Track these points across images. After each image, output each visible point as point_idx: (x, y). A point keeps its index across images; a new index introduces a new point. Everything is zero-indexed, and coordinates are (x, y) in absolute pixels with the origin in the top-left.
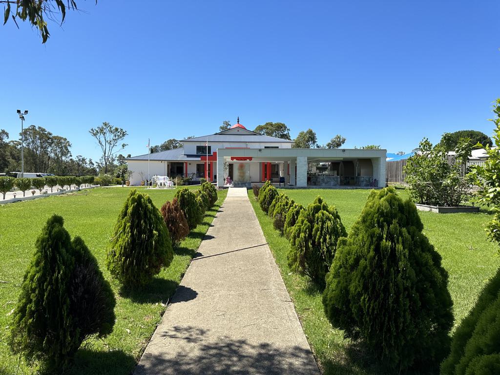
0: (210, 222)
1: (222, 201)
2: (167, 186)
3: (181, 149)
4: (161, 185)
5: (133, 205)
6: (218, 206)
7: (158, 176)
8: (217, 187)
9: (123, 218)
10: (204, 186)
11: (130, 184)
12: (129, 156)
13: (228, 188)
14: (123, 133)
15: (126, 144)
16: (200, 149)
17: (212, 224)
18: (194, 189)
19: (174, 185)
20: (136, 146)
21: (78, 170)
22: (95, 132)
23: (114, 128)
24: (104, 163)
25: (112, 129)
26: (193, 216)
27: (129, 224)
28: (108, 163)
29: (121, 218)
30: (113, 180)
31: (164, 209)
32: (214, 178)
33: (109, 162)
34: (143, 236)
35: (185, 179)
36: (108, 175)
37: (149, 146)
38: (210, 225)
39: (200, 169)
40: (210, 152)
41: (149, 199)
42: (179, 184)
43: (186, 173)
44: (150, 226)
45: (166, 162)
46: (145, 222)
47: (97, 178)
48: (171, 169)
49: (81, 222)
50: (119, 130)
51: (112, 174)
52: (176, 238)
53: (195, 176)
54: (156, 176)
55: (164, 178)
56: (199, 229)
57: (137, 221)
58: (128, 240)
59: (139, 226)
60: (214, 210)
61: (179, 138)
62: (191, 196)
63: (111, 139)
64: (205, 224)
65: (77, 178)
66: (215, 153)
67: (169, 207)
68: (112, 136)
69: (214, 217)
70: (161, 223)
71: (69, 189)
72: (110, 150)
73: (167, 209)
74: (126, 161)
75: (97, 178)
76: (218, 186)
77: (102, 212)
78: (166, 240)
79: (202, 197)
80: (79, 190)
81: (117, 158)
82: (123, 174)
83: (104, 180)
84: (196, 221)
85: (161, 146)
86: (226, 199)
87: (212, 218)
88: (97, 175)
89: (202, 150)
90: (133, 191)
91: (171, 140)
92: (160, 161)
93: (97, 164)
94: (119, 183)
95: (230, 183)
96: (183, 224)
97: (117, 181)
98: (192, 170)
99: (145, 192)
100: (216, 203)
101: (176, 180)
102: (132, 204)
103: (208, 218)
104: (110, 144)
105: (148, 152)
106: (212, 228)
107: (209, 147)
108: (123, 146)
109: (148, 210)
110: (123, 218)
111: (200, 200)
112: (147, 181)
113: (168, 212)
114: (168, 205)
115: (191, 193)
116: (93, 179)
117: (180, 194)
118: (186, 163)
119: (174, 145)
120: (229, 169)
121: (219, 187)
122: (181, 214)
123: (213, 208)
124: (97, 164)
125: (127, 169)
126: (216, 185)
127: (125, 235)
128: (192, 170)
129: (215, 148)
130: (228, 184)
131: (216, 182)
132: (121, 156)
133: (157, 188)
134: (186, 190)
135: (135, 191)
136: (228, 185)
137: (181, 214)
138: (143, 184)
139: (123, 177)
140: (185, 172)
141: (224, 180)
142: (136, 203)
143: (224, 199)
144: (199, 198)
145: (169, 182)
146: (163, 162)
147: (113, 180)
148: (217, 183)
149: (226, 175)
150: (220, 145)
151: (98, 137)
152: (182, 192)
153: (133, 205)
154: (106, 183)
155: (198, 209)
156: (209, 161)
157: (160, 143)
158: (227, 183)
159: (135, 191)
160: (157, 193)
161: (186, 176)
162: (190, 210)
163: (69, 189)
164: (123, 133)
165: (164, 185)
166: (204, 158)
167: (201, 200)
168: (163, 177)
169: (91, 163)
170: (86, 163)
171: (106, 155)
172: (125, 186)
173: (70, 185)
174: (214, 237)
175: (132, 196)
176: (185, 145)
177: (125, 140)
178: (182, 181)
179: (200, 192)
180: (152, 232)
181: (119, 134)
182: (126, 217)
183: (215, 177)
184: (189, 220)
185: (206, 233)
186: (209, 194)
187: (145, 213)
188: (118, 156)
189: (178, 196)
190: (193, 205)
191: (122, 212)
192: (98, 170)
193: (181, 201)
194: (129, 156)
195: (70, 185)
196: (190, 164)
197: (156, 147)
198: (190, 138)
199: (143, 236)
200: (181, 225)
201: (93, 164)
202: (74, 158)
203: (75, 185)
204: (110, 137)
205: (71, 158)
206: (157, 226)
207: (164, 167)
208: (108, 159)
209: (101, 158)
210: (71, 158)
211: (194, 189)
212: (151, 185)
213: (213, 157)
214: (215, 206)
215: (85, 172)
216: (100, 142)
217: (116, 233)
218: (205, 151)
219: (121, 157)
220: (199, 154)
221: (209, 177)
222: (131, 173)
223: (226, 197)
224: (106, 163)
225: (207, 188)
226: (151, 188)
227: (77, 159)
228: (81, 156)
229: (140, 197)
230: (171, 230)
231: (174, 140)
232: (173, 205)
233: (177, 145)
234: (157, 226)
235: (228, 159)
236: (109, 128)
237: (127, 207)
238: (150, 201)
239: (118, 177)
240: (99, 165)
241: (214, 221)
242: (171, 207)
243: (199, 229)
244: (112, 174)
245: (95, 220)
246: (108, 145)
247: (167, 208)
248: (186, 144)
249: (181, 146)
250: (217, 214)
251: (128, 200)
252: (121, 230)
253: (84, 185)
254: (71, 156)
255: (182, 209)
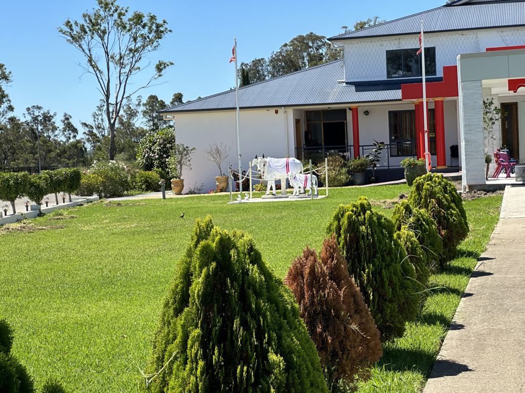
0: (448, 315)
1: (485, 236)
2: (296, 190)
3: (337, 65)
4: (278, 187)
5: (204, 270)
6: (470, 254)
7: (268, 159)
8: (462, 188)
9: (178, 312)
10: (419, 188)
11: (185, 190)
12: (178, 98)
13: (502, 187)
14: (158, 26)
15: (166, 61)
16: (402, 63)
17: (457, 320)
18: (386, 200)
19: (320, 184)
20: (194, 69)
21: (33, 151)
22: (76, 29)
23: (130, 15)
24: (106, 124)
25: (125, 19)
26: (389, 295)
27: (196, 332)
28: (117, 125)
29: (171, 311)
30: (133, 177)
31: (296, 274)
32: (450, 157)
33: (121, 123)
34: (241, 370)
35: (353, 163)
36: (120, 163)
37: (234, 59)
38: (450, 325)
39: (402, 126)
40: (431, 69)
41: (251, 249)
42: (334, 183)
43: (357, 145)
44: (260, 338)
45: (290, 111)
46: (244, 324)
47: (89, 174)
48: (306, 133)
49: (52, 316)
50: (145, 20)
51: (132, 157)
52: (341, 372)
53: (385, 153)
54: (260, 159)
55: (287, 165)
56: (414, 337)
57: (219, 322)
58: (197, 385)
59: (225, 337)
60: (459, 271)
61: (328, 31)
62: (381, 227)
63: (124, 48)
64: (431, 319)
65: (33, 178)
66: (451, 71)
67: (312, 269)
68: (126, 37)
69: (460, 294)
70: (293, 327)
71: (10, 212)
72: (123, 84)
73: (307, 276)
74: (169, 116)
75: (89, 174)
76: (464, 182)
77: (109, 281)
78: (312, 385)
79: (418, 225)
80: (41, 214)
81: (142, 108)
82: (161, 157)
83: (111, 179)
84: (401, 310)
85: (271, 61)
86: (499, 228)
87: (453, 298)
88: (87, 163)
89: (402, 63)
90: (203, 224)
91: (301, 39)
92: (273, 110)
93: (87, 130)
94: (151, 186)
95: (509, 170)
96: (360, 325)
97: (146, 181)
98: (373, 132)
99: (236, 219)
100: (463, 246)
101: (325, 169)
102: (201, 268)
103: (439, 298)
104: (122, 65)
105: (234, 81)
106: (456, 332)
107: (431, 52)
108: (160, 68)
109: (252, 284)
110: (178, 312)
111: (408, 238)
112: (236, 177)
113: (311, 286)
114: (309, 264)
115: (379, 218)
116: (76, 177)
117: (345, 221)
118: (355, 111)
119: (313, 51)
120: (504, 120)
121: (471, 187)
122: (351, 294)
123: (455, 263)
124: (87, 130)
125: (171, 140)
126: (459, 178)
127: (188, 366)
128: (373, 132)
129: (448, 53)
130: (503, 175)
131: (458, 169)
132: (153, 98)
133: (266, 198)
134: (364, 208)
135: (209, 226)
136: (502, 179)
137: (351, 294)
138: (223, 185)
139: (163, 165)
140: (351, 141)
141: (488, 161)
142: (214, 264)
143: (491, 228)
144: (405, 231)
145: (303, 176)
146: (281, 111)
147: (133, 177)
148: (463, 173)
149: (493, 143)
150: (466, 43)
151: (85, 47)
152: (350, 217)
153: (204, 270)
154: (115, 187)
155: (406, 271)
156: (431, 100)
157: (266, 48)
158: (498, 172)
159: (209, 226)
160: (268, 216)
161: (357, 154)
162: (380, 273)
163: (10, 212)
164: (158, 26)
165: (289, 186)
166: (411, 89)
167: (415, 239)
168: (284, 160)
169: (69, 127)
170: (54, 129)
171: (112, 100)
172: (170, 194)
173: (12, 200)
174: (465, 368)
175: (203, 243)
176: (346, 50)
177: (164, 50)
178: (344, 170)
179: (407, 208)
180: (266, 358)
181: (145, 31)
182: (186, 309)
183: (455, 151)
184: (379, 310)
185: (437, 352)
186: (437, 215)
187: (243, 297)
188: (144, 100)
189: (339, 228)
190: (388, 259)
191: (174, 292)
192: (88, 146)
193: (349, 246)
194: (178, 98)
195: (12, 200)
196: (367, 113)
197: (258, 63)
198: (361, 26)
199: (241, 370)
200: (354, 327)
201: (75, 130)
202: (22, 116)
203: (26, 199)
204: (119, 42)
205: (10, 114)
206: (280, 338)
207: (284, 128)
208: (117, 113)
209: (95, 110)
210: (10, 114)
211: (386, 200)
212: (246, 187)
213: (446, 84)
214: (462, 254)
215: (53, 154)
216: (90, 61)
217: (161, 360)
218: (413, 65)
219: (155, 106)
220: (396, 78)
221: (433, 151)
222: (185, 151)
223: (495, 220)
224: (112, 126)
225: (432, 194)
226: (249, 198)
227: (29, 118)
228: (39, 108)
229: (226, 244)
230: (322, 346)
231: (313, 37)
232: (325, 263)
233: (323, 51)
234: (280, 338)
235: (499, 89)
236: (116, 15)
237: (187, 278)
238: (256, 258)
239: (148, 167)
240: (91, 134)
241: (461, 311)
242: (318, 270)
243: (414, 337)
244: (132, 157)
245: (92, 309)
246: (114, 69)
247: (307, 271)
248: (350, 48)
249: (334, 57)
250: (472, 284)
251: (190, 254)
252: (174, 349)
253: (51, 196)
254: (11, 108)
255: (352, 271)
